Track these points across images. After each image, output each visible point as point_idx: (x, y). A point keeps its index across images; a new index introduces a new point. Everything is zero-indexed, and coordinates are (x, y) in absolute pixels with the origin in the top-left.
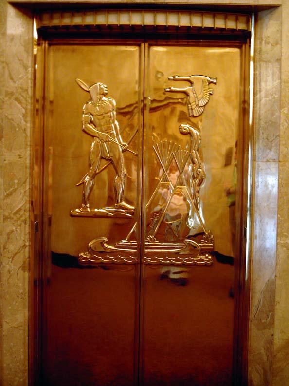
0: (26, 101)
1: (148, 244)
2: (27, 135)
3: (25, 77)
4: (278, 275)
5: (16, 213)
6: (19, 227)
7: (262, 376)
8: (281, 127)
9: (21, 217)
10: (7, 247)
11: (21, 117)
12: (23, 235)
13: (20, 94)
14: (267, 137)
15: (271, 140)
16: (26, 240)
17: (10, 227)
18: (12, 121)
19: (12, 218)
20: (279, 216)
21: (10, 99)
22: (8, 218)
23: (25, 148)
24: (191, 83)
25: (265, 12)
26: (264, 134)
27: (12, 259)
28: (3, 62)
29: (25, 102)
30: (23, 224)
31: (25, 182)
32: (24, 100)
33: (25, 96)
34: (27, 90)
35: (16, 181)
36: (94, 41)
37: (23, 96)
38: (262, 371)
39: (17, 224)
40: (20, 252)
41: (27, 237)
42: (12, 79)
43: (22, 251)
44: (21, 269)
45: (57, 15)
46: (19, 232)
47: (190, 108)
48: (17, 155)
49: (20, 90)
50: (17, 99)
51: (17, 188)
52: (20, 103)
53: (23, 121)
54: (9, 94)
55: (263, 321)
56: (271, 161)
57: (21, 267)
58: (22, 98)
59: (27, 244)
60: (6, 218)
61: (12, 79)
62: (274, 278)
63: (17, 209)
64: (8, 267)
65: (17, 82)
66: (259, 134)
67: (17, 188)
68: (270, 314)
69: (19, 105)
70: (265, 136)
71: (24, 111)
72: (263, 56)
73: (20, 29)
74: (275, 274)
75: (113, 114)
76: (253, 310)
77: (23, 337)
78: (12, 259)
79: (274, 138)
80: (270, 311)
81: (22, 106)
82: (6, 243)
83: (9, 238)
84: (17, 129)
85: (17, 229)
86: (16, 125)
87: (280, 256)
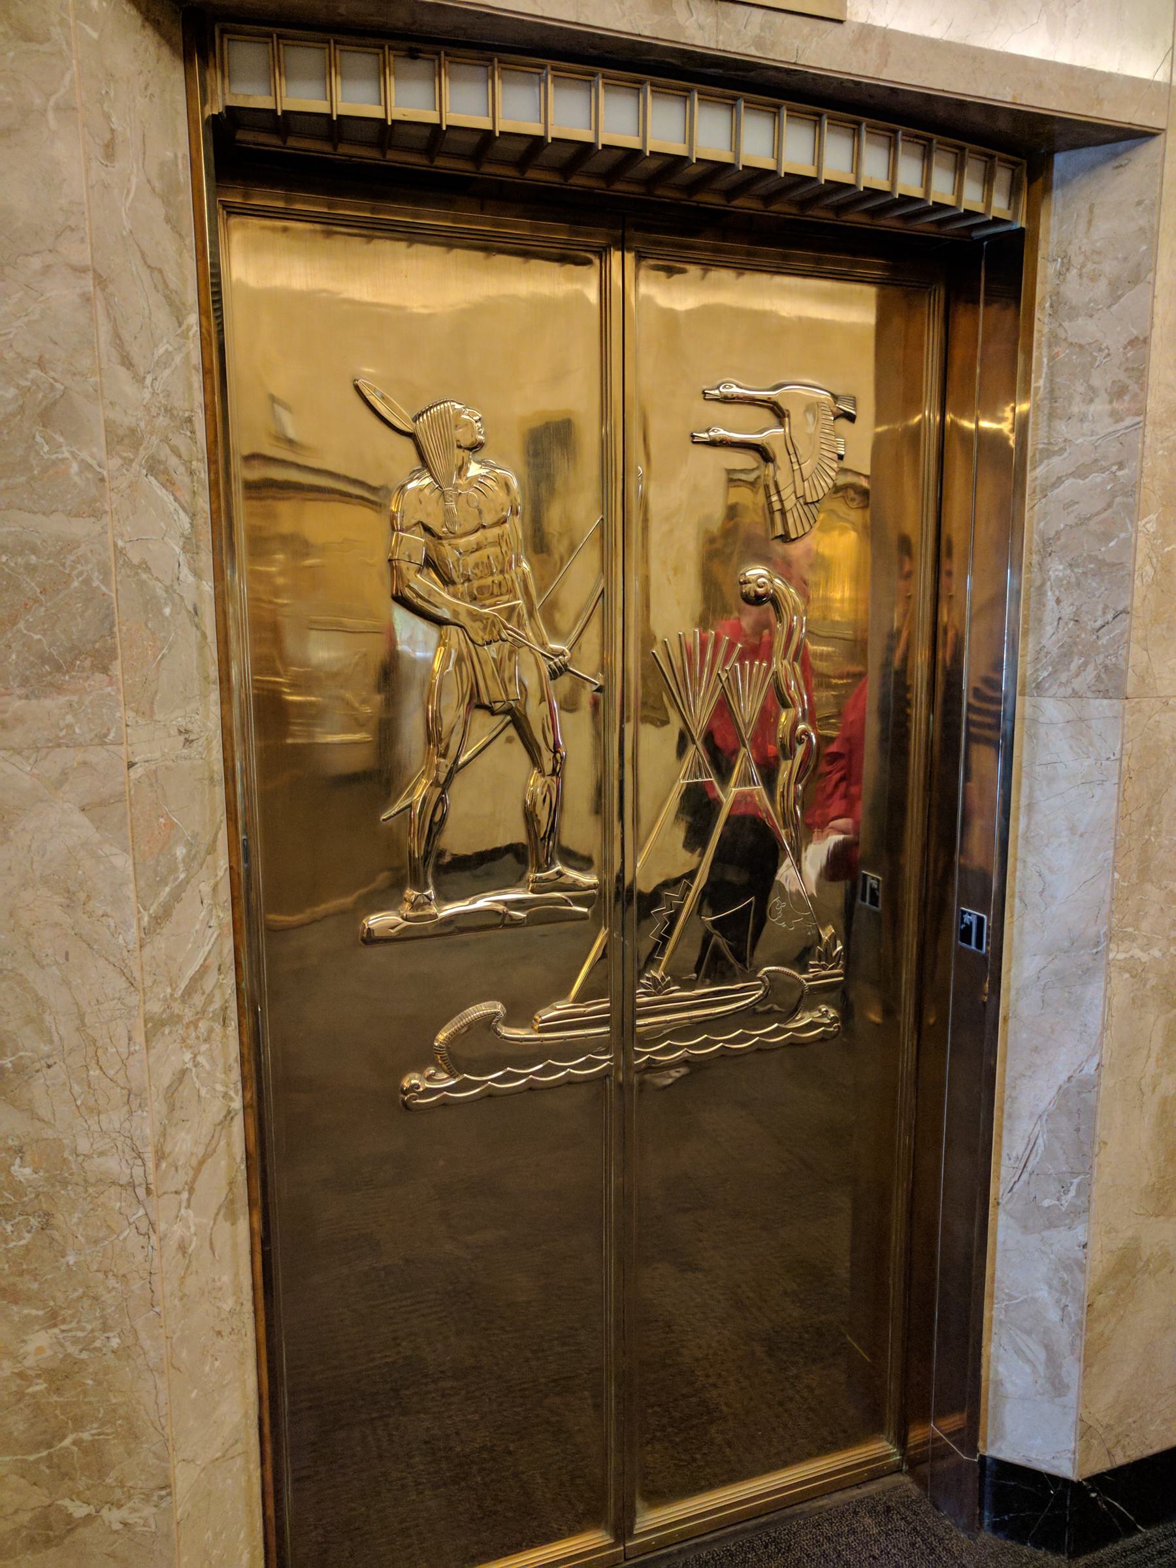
0: (192, 473)
1: (646, 999)
2: (204, 636)
3: (178, 359)
4: (1105, 1062)
5: (189, 992)
6: (204, 1047)
7: (1041, 1369)
8: (1138, 583)
9: (210, 999)
10: (167, 1149)
11: (178, 550)
12: (220, 1075)
13: (166, 440)
14: (1075, 614)
15: (1092, 625)
16: (232, 1093)
17: (173, 1056)
18: (144, 576)
19: (179, 1018)
20: (1117, 876)
21: (128, 462)
22: (163, 1024)
23: (204, 696)
24: (779, 413)
25: (1085, 155)
26: (1064, 604)
27: (191, 1191)
28: (80, 270)
29: (187, 479)
30: (218, 1027)
31: (212, 849)
32: (181, 469)
33: (183, 451)
34: (189, 420)
35: (180, 852)
36: (373, 211)
37: (176, 451)
38: (1042, 1355)
39: (198, 1038)
40: (214, 1151)
41: (236, 1074)
42: (127, 362)
43: (223, 1143)
44: (221, 1217)
45: (305, 57)
46: (207, 1067)
47: (777, 506)
48: (174, 732)
49: (162, 421)
50: (154, 467)
51: (187, 881)
52: (169, 483)
53: (185, 570)
54: (121, 441)
55: (1046, 1203)
56: (1089, 694)
57: (221, 1206)
58: (173, 461)
59: (237, 1104)
60: (155, 1026)
61: (127, 362)
62: (1092, 1072)
63: (190, 972)
64: (178, 1230)
65: (148, 381)
66: (1041, 604)
67: (187, 881)
68: (1076, 1181)
69: (162, 493)
70: (1067, 611)
71: (185, 520)
72: (1066, 324)
73: (124, 117)
74: (1096, 1060)
75: (1053, 593)
76: (1003, 1172)
77: (243, 1478)
78: (191, 1191)
79: (1109, 617)
80: (1074, 1174)
81: (176, 499)
82: (164, 1134)
83: (172, 1108)
84: (167, 611)
85: (200, 1059)
86: (160, 592)
87: (1115, 1002)
